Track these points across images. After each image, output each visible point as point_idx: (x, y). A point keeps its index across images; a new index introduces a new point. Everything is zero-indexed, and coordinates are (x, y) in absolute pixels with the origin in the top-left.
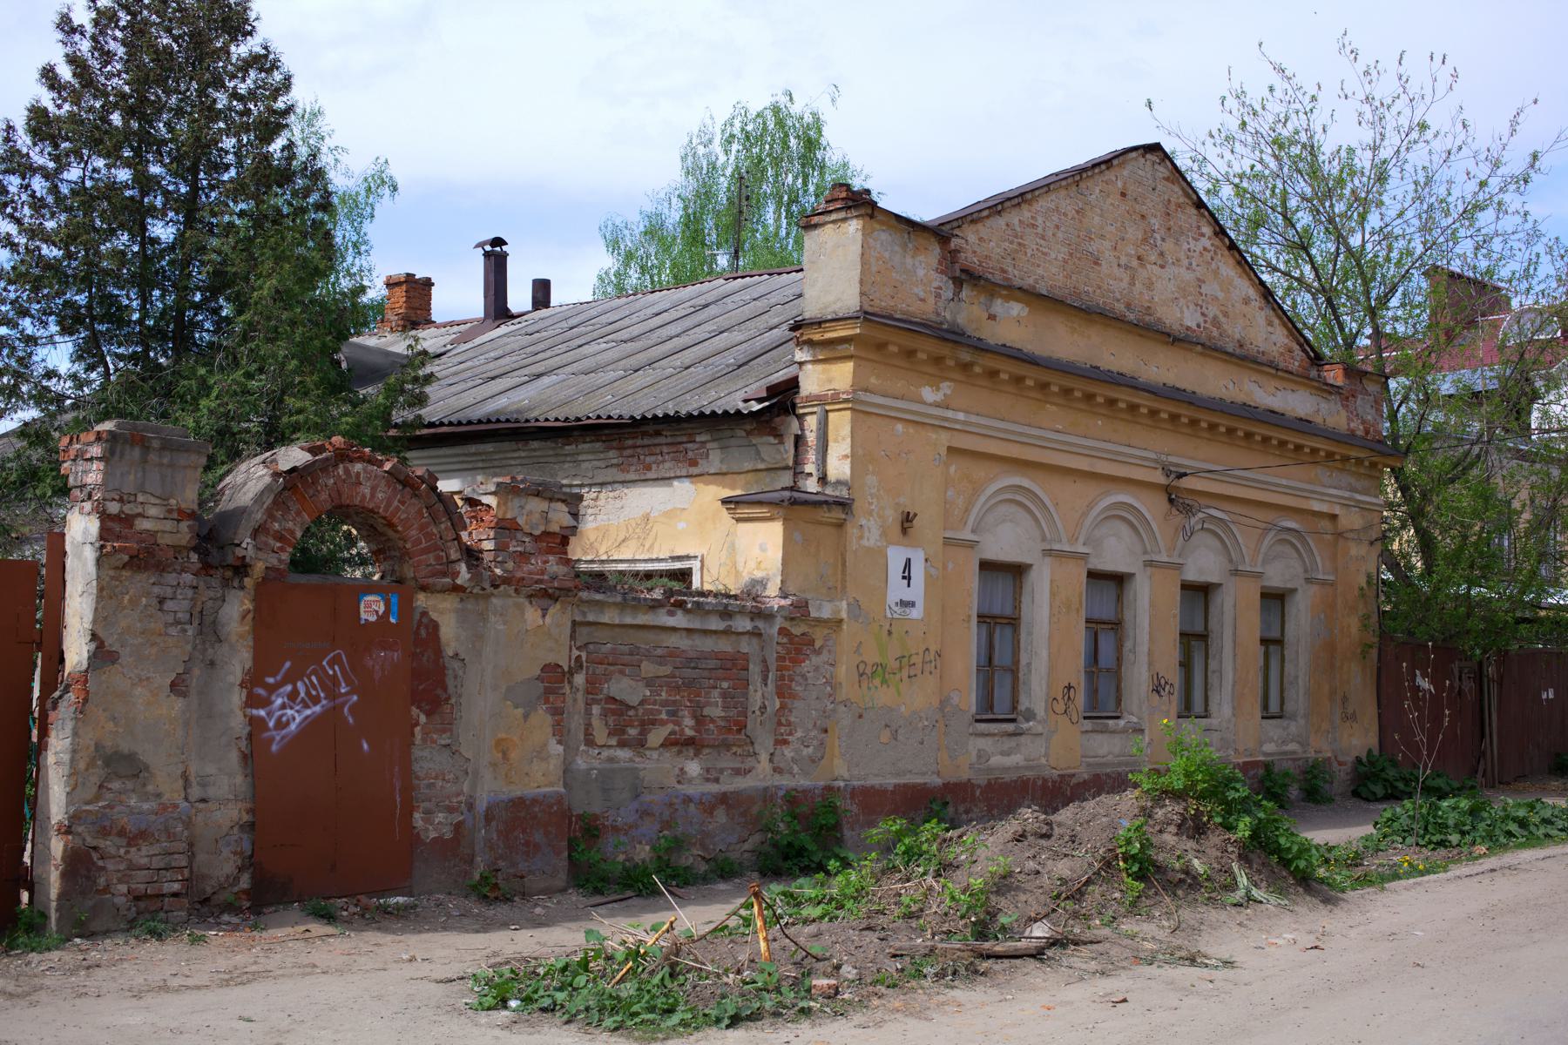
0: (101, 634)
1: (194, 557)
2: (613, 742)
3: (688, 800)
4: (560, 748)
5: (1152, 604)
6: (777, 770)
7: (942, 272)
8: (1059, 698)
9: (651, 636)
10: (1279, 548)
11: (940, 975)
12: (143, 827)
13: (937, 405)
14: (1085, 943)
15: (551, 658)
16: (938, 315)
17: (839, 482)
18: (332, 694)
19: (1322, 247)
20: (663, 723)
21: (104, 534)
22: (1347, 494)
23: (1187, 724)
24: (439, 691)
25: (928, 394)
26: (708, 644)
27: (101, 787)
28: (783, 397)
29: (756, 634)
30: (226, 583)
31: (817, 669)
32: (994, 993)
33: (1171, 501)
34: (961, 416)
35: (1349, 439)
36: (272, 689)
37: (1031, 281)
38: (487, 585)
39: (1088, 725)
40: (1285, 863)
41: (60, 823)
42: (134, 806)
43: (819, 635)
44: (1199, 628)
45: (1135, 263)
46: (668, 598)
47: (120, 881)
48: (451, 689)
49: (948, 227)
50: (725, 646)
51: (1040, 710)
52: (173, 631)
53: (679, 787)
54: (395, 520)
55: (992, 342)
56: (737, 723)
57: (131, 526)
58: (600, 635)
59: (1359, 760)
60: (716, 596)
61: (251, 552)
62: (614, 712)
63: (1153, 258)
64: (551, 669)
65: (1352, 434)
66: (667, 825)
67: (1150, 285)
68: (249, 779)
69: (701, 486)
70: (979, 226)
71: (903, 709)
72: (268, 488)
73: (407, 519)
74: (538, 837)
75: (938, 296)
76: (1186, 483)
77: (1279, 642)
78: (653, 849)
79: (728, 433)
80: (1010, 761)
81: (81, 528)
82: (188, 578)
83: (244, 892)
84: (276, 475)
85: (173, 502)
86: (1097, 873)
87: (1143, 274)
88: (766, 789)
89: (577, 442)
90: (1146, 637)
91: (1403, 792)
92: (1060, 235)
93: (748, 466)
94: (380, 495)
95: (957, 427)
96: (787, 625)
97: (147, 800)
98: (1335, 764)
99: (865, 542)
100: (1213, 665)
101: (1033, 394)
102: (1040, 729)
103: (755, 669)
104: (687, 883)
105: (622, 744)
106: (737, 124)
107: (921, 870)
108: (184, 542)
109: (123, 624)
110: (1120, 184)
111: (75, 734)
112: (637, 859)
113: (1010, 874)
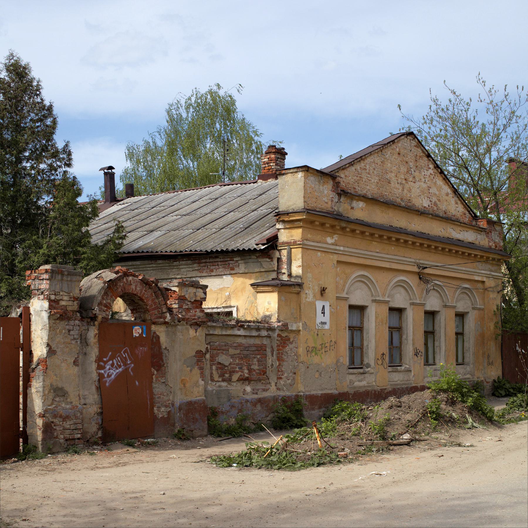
0: (50, 344)
1: (78, 314)
2: (220, 380)
3: (247, 401)
4: (203, 382)
5: (413, 320)
6: (278, 389)
7: (333, 191)
8: (380, 358)
9: (232, 339)
10: (462, 296)
11: (378, 451)
12: (68, 414)
13: (333, 244)
14: (422, 441)
15: (199, 348)
16: (332, 208)
17: (297, 277)
18: (125, 364)
19: (474, 166)
20: (237, 372)
21: (51, 307)
22: (489, 273)
23: (428, 368)
24: (161, 362)
25: (329, 240)
26: (252, 341)
27: (53, 400)
28: (273, 242)
29: (269, 337)
30: (88, 324)
31: (291, 349)
32: (397, 456)
33: (420, 278)
34: (342, 248)
35: (489, 250)
36: (105, 363)
37: (365, 192)
38: (176, 321)
39: (390, 369)
40: (484, 414)
41: (40, 413)
42: (64, 407)
43: (292, 336)
44: (430, 329)
45: (404, 182)
46: (238, 324)
47: (61, 434)
48: (165, 361)
49: (334, 172)
50: (257, 341)
51: (372, 363)
52: (73, 342)
53: (244, 396)
54: (144, 298)
55: (352, 218)
56: (263, 371)
57: (58, 304)
58: (214, 339)
59: (494, 381)
60: (254, 322)
61: (98, 312)
62: (220, 368)
63: (411, 179)
64: (199, 352)
65: (490, 248)
66: (240, 411)
67: (410, 191)
68: (99, 396)
69: (236, 278)
70: (345, 171)
71: (323, 364)
72: (103, 288)
73: (147, 297)
74: (197, 416)
75: (332, 201)
76: (426, 271)
77: (462, 334)
78: (236, 420)
79: (248, 257)
80: (364, 383)
81: (38, 306)
82: (77, 322)
83: (100, 438)
84: (105, 282)
85: (72, 294)
86: (421, 418)
87: (407, 186)
88: (274, 396)
89: (179, 261)
90: (412, 334)
91: (512, 393)
92: (375, 172)
93: (257, 270)
94: (138, 289)
95: (341, 253)
96: (280, 333)
97: (68, 404)
98: (485, 383)
99: (308, 300)
100: (437, 344)
101: (368, 238)
102: (372, 371)
103: (269, 350)
104: (249, 433)
105: (223, 380)
106: (193, 99)
107: (356, 420)
108: (76, 309)
109: (57, 340)
110: (398, 150)
111: (44, 381)
112: (230, 424)
113: (389, 420)
